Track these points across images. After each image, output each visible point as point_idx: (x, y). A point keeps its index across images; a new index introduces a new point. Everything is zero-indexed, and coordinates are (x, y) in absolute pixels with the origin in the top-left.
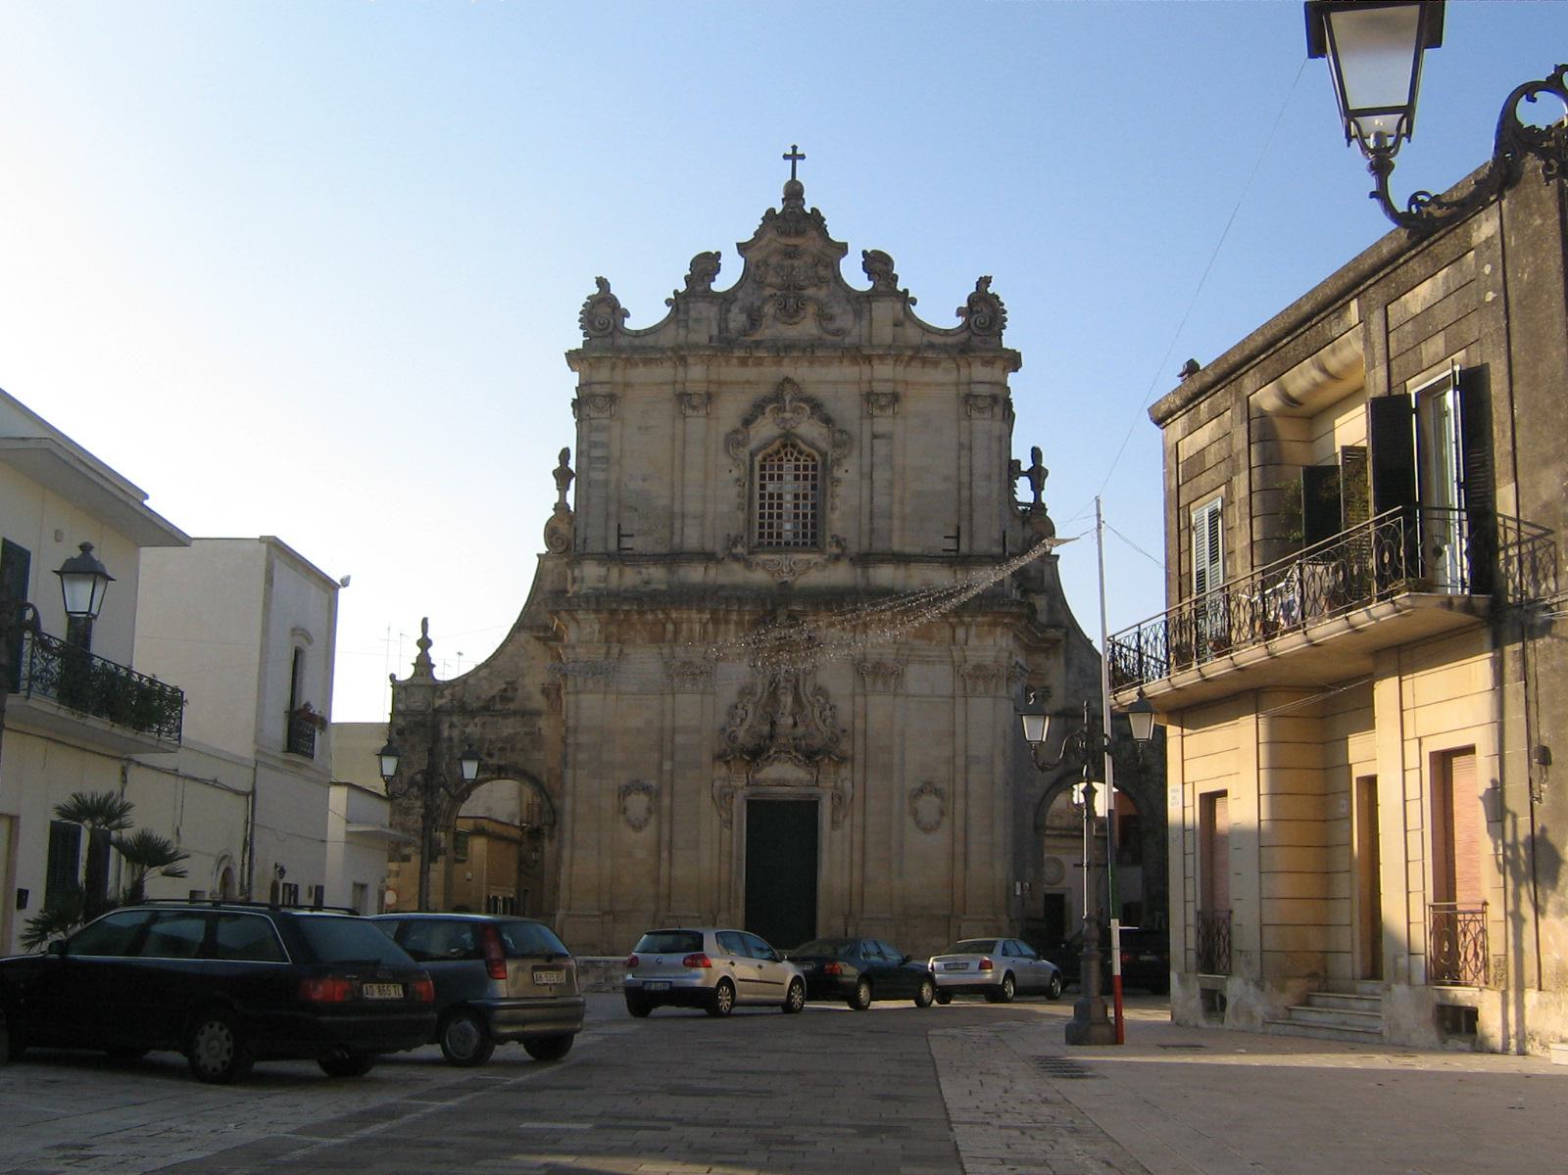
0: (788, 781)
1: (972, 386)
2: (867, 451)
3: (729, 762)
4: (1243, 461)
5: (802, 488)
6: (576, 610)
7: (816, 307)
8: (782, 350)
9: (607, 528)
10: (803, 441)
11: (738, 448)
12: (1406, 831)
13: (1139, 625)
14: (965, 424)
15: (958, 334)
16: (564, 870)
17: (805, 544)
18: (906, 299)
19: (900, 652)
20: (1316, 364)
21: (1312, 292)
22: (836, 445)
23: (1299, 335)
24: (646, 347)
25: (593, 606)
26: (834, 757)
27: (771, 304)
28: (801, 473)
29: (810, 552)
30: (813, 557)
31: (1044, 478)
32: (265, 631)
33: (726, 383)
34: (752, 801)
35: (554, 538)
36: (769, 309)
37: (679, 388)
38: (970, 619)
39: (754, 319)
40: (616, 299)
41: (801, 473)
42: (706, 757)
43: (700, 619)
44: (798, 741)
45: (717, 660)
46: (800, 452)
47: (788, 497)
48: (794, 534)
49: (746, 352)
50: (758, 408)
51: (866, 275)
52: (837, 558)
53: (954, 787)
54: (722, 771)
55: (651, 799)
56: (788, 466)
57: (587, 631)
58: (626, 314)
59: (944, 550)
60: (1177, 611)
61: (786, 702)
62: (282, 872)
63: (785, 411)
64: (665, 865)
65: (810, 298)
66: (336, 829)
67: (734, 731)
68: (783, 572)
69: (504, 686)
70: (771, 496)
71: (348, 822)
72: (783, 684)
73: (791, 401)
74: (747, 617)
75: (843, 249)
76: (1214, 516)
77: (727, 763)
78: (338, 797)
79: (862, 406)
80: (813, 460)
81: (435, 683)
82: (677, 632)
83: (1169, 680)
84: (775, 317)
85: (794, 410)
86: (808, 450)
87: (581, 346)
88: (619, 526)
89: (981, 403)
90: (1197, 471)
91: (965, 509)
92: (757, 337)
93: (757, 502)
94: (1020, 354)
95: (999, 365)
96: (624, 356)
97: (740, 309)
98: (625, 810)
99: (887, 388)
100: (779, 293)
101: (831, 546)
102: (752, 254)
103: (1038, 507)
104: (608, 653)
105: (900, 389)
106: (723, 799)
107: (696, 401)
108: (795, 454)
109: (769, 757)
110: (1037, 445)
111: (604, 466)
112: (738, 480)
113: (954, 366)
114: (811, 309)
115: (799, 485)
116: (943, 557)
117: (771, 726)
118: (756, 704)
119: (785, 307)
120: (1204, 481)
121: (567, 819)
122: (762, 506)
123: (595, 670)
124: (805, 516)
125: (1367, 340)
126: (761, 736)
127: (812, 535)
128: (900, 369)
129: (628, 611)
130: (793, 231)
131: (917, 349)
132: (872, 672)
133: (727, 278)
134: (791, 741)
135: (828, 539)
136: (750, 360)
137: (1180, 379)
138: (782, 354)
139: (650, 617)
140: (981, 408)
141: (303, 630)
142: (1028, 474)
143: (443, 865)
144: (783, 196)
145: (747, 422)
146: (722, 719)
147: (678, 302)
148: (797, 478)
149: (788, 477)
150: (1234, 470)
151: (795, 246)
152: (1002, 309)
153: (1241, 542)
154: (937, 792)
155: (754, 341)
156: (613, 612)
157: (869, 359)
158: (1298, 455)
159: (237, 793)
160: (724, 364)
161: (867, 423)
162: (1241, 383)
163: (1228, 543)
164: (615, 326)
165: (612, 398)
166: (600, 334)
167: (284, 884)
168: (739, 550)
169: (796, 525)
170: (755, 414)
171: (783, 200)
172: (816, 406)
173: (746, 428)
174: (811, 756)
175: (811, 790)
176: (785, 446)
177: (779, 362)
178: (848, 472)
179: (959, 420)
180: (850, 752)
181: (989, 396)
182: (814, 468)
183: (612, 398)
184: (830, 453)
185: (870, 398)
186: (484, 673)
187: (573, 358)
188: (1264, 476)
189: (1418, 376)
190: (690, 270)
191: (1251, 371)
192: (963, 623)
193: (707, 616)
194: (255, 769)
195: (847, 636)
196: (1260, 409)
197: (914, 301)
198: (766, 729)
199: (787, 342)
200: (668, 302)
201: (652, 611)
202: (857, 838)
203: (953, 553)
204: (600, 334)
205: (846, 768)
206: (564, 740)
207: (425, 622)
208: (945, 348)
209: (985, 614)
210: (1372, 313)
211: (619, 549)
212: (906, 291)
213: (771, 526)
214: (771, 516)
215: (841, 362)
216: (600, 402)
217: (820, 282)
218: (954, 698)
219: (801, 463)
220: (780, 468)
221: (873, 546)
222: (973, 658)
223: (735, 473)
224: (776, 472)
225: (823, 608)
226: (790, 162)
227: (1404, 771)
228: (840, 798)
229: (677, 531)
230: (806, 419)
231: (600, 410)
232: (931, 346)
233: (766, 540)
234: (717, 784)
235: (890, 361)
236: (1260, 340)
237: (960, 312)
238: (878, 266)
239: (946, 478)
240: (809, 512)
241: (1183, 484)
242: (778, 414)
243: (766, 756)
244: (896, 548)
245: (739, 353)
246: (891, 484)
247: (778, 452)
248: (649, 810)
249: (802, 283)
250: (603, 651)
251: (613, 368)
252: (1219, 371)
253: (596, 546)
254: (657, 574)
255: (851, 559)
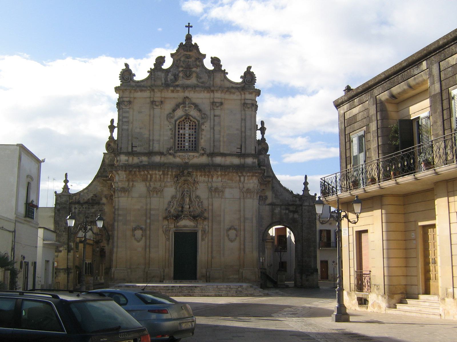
0: (188, 226)
1: (246, 100)
2: (212, 121)
3: (168, 220)
4: (374, 118)
5: (191, 132)
6: (118, 171)
7: (196, 75)
8: (185, 87)
9: (128, 144)
10: (192, 117)
11: (171, 119)
12: (451, 245)
13: (336, 174)
14: (243, 112)
15: (240, 84)
16: (114, 255)
17: (192, 150)
18: (224, 73)
19: (223, 184)
20: (406, 84)
21: (407, 59)
22: (202, 118)
23: (399, 75)
24: (141, 85)
25: (124, 169)
26: (202, 218)
27: (182, 73)
28: (191, 127)
29: (194, 152)
30: (195, 154)
31: (265, 130)
32: (19, 177)
33: (167, 98)
34: (176, 232)
35: (109, 147)
36: (181, 75)
37: (152, 99)
38: (245, 174)
39: (176, 77)
40: (131, 70)
41: (191, 127)
42: (161, 218)
43: (159, 174)
44: (191, 213)
45: (164, 187)
46: (191, 121)
47: (187, 135)
48: (189, 147)
49: (174, 88)
50: (178, 106)
51: (212, 65)
52: (203, 154)
53: (240, 227)
54: (166, 223)
55: (143, 232)
56: (187, 125)
57: (122, 177)
58: (134, 75)
59: (237, 152)
60: (345, 171)
61: (187, 201)
62: (24, 258)
63: (186, 107)
64: (148, 253)
65: (194, 72)
66: (40, 243)
67: (170, 210)
68: (186, 159)
69: (92, 195)
70: (181, 134)
71: (44, 240)
72: (186, 195)
73: (188, 104)
74: (174, 173)
75: (204, 56)
76: (360, 138)
77: (168, 220)
78: (41, 232)
79: (210, 106)
80: (195, 123)
81: (69, 194)
82: (151, 178)
83: (350, 192)
84: (183, 77)
85: (189, 107)
86: (193, 120)
87: (120, 85)
88: (132, 143)
89: (248, 106)
90: (353, 122)
91: (243, 139)
92: (177, 83)
93: (177, 136)
94: (260, 91)
95: (254, 94)
96: (134, 89)
97: (171, 74)
98: (134, 236)
99: (219, 100)
100: (184, 70)
101: (201, 151)
102: (175, 57)
103: (263, 139)
104: (129, 184)
105: (223, 101)
106: (166, 232)
107: (157, 104)
108: (189, 121)
109: (181, 218)
110: (263, 120)
111: (127, 124)
112: (171, 129)
113: (240, 94)
114: (194, 75)
115: (190, 131)
116: (236, 154)
117: (182, 208)
118: (177, 201)
119: (186, 74)
120: (356, 125)
121: (116, 238)
122: (179, 138)
123: (124, 190)
124: (192, 141)
125: (431, 75)
126: (179, 211)
127: (195, 147)
128: (223, 94)
129: (135, 171)
130: (189, 50)
131: (228, 88)
132: (214, 191)
133: (168, 64)
134: (188, 213)
135: (200, 148)
136: (175, 91)
137: (344, 92)
138: (185, 89)
139: (142, 173)
140: (248, 108)
141: (31, 176)
142: (260, 129)
143: (73, 253)
144: (185, 39)
145: (174, 111)
146: (166, 206)
147: (151, 72)
148: (190, 129)
149: (187, 129)
150: (371, 121)
151: (190, 55)
152: (255, 76)
153: (374, 145)
154: (235, 229)
155: (176, 85)
156: (130, 171)
157: (213, 91)
158: (394, 116)
159: (10, 231)
160: (166, 92)
161: (212, 111)
162: (373, 92)
163: (367, 146)
164: (131, 79)
165: (130, 102)
166: (126, 82)
167: (24, 262)
168: (171, 151)
169: (189, 144)
170: (177, 108)
171: (185, 40)
172: (196, 106)
173: (174, 113)
174: (195, 218)
175: (196, 229)
176: (186, 119)
177: (184, 92)
178: (206, 127)
179: (241, 111)
180: (207, 216)
181: (251, 104)
182: (195, 126)
183: (130, 102)
184: (200, 121)
185: (213, 103)
186: (85, 191)
187: (117, 89)
188: (382, 123)
189: (454, 86)
190: (156, 61)
191: (377, 88)
192: (243, 175)
193: (161, 173)
194: (15, 223)
195: (206, 179)
196: (380, 100)
197: (227, 73)
198: (180, 209)
199: (187, 85)
200: (148, 72)
201: (143, 171)
202: (210, 244)
203: (240, 153)
204: (126, 82)
205: (206, 221)
206: (114, 213)
207: (66, 175)
208: (237, 88)
209: (250, 173)
210: (432, 65)
211: (132, 151)
212: (225, 70)
213: (181, 144)
214: (181, 141)
215: (204, 92)
216: (126, 103)
217: (197, 66)
218: (240, 199)
219: (191, 124)
220: (184, 125)
221: (215, 151)
222: (247, 186)
223: (170, 127)
224: (183, 127)
225: (199, 170)
226: (188, 28)
227: (450, 223)
228: (204, 232)
229: (151, 145)
230: (193, 110)
231: (126, 106)
232: (232, 87)
233: (180, 149)
234: (165, 227)
235: (219, 92)
236: (383, 76)
237: (241, 77)
238: (216, 62)
239: (237, 130)
240: (194, 139)
241: (347, 126)
242: (184, 108)
243: (180, 218)
244: (222, 151)
245: (172, 88)
246: (220, 131)
247: (184, 121)
248: (142, 236)
249: (192, 67)
250: (127, 184)
251: (130, 92)
252: (364, 87)
253: (124, 150)
254: (145, 159)
255: (207, 155)
